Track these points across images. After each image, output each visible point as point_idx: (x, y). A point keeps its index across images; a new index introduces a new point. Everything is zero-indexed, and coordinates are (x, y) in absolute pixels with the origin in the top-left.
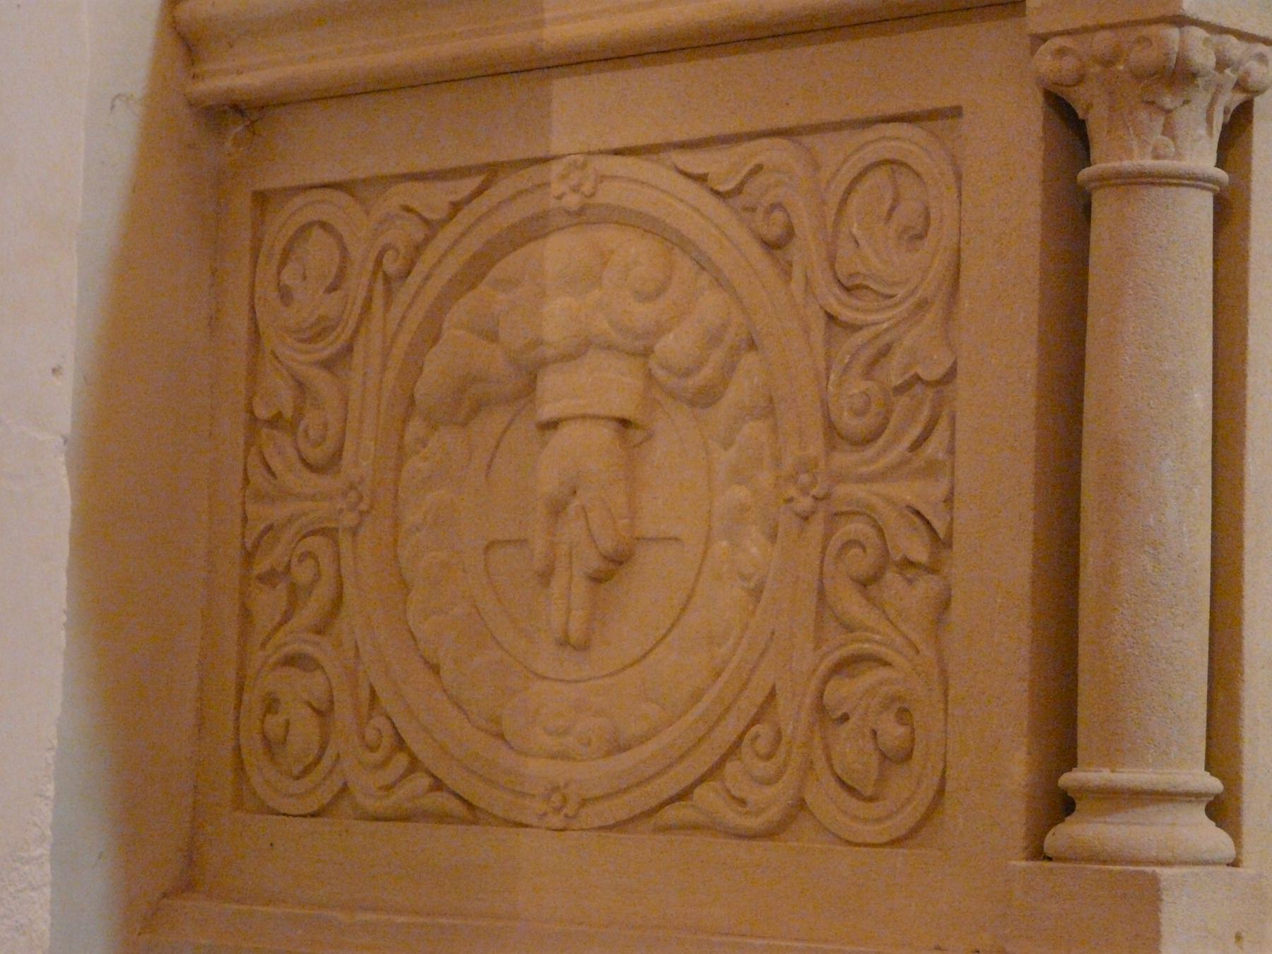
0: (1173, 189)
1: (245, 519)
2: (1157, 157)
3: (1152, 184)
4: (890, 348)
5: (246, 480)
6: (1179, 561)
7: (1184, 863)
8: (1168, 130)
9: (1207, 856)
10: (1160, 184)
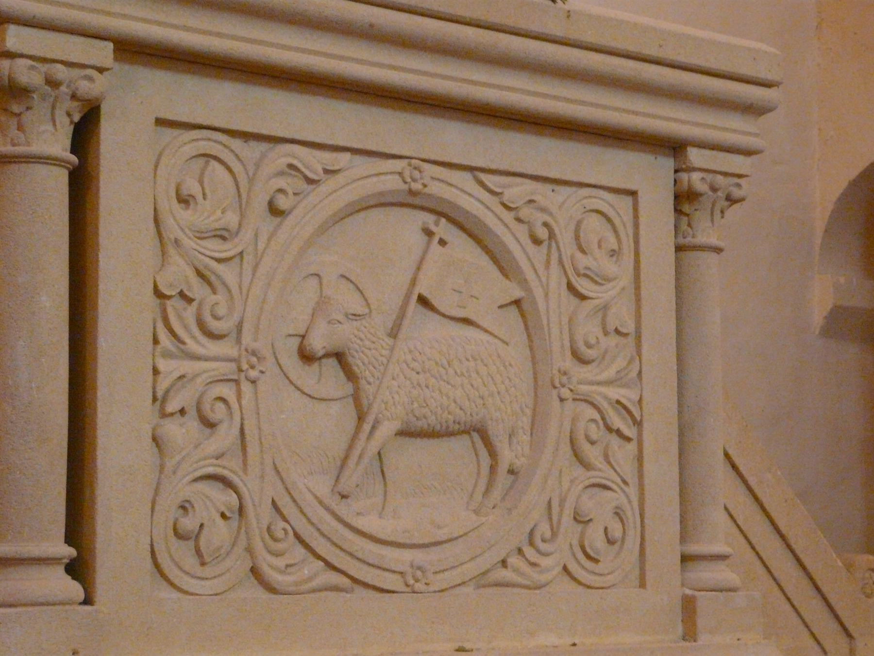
0: (24, 165)
1: (156, 372)
2: (14, 145)
3: (10, 162)
4: (676, 210)
5: (156, 341)
6: (30, 407)
7: (25, 605)
8: (20, 128)
9: (41, 600)
10: (15, 162)
